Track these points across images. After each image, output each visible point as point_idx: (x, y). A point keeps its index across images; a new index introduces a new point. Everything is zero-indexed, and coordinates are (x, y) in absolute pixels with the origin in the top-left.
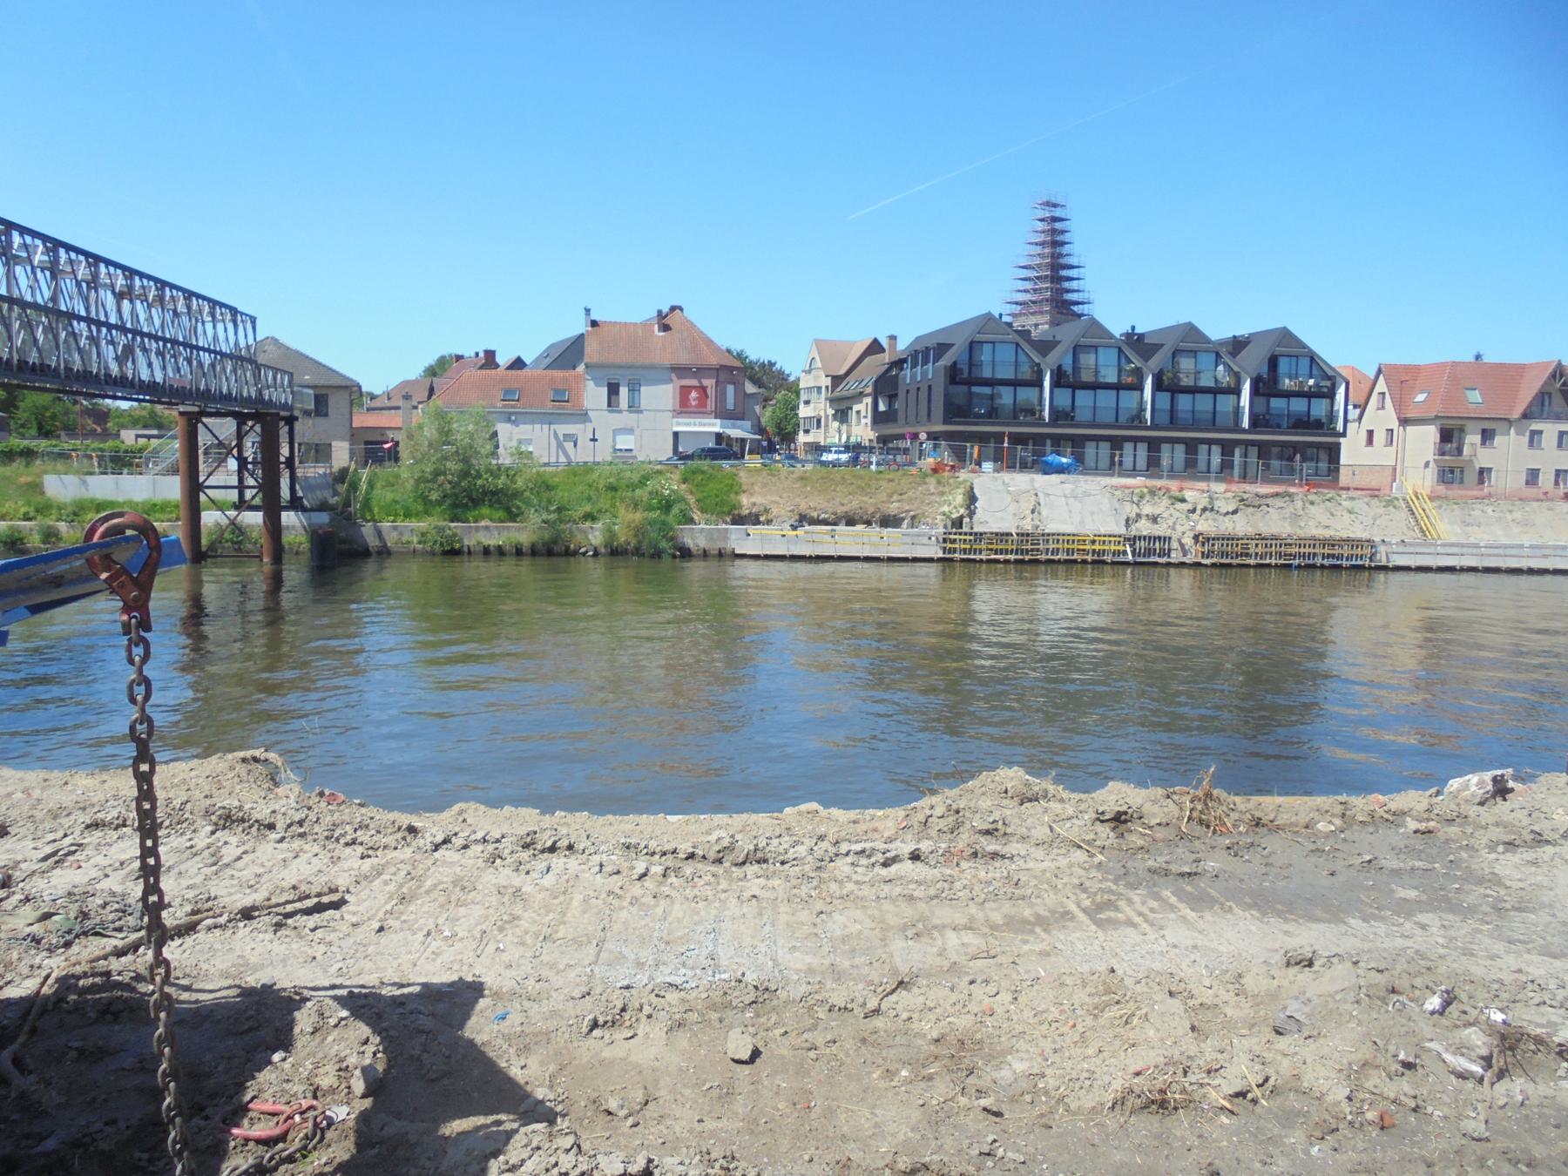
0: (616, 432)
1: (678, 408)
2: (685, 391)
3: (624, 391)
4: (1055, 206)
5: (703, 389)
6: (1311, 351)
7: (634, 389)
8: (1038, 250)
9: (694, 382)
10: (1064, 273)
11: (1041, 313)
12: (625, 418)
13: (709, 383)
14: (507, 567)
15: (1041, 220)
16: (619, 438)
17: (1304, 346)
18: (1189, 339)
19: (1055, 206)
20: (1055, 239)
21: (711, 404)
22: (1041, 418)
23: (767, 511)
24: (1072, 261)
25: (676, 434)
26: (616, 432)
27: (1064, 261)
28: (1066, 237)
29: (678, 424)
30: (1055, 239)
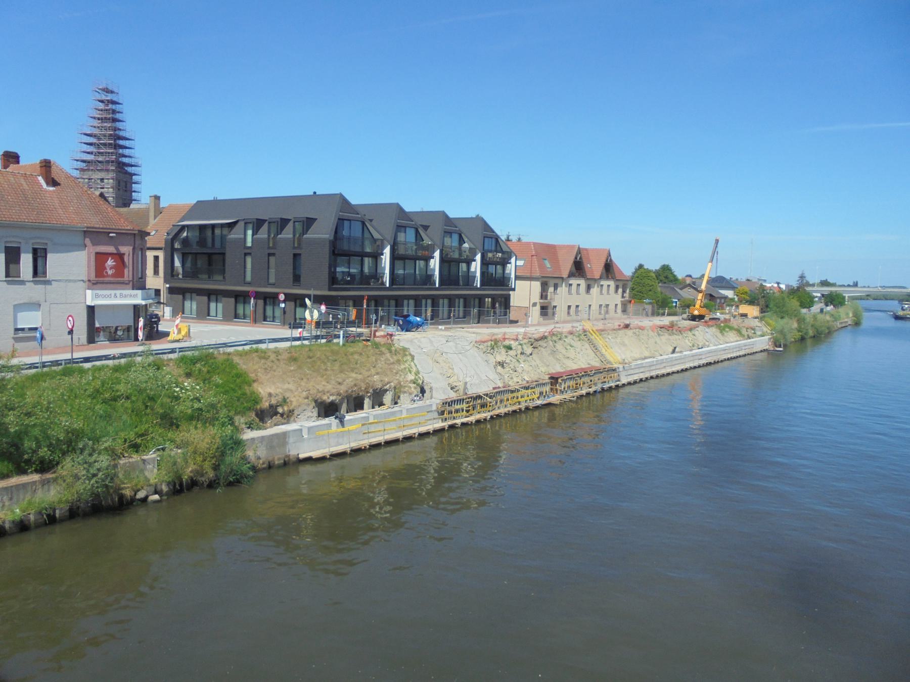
0: (18, 308)
1: (93, 277)
2: (100, 258)
3: (26, 260)
4: (112, 92)
5: (119, 257)
6: (497, 235)
7: (39, 255)
8: (96, 123)
9: (111, 249)
10: (121, 142)
11: (107, 170)
12: (31, 291)
13: (126, 250)
14: (56, 539)
15: (102, 101)
16: (21, 315)
17: (493, 232)
18: (346, 214)
19: (112, 92)
20: (110, 113)
21: (128, 273)
22: (383, 283)
23: (285, 400)
24: (127, 135)
25: (91, 310)
26: (18, 308)
27: (121, 133)
28: (118, 116)
29: (97, 296)
30: (110, 113)
